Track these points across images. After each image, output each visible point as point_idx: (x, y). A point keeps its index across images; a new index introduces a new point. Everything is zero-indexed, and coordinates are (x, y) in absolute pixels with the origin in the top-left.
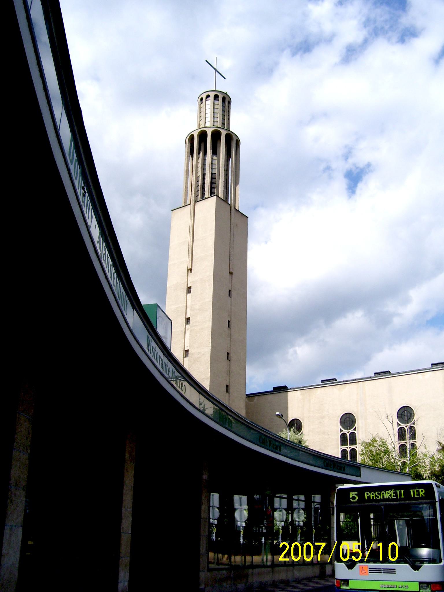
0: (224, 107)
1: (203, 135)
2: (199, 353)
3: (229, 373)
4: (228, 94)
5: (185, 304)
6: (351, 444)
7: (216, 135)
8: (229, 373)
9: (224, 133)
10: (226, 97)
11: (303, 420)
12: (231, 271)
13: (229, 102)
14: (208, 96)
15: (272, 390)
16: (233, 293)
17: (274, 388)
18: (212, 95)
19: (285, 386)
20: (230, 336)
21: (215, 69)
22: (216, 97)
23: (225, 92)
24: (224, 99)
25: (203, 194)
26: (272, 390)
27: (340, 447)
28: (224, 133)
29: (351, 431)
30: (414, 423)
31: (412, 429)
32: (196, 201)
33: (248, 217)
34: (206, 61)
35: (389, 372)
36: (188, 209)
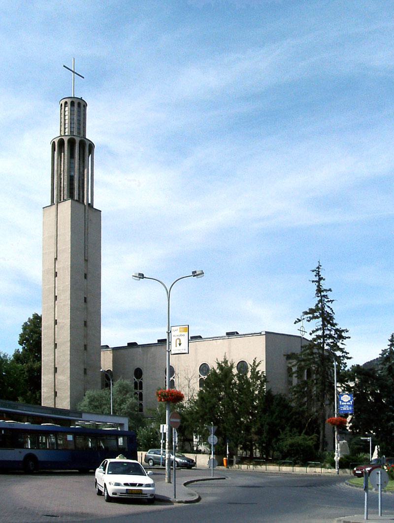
0: (79, 112)
1: (61, 142)
2: (64, 323)
3: (86, 336)
4: (83, 99)
5: (54, 286)
6: (140, 389)
7: (72, 142)
8: (86, 336)
9: (77, 140)
10: (81, 102)
11: (143, 369)
12: (86, 258)
13: (84, 106)
14: (66, 103)
15: (127, 345)
16: (89, 276)
17: (128, 344)
18: (69, 101)
19: (135, 343)
20: (87, 308)
21: (73, 72)
22: (72, 103)
23: (80, 98)
24: (79, 104)
25: (61, 200)
26: (127, 345)
27: (199, 388)
28: (77, 140)
29: (140, 380)
30: (142, 379)
31: (141, 383)
32: (58, 203)
33: (101, 211)
34: (64, 66)
35: (200, 337)
36: (54, 207)
